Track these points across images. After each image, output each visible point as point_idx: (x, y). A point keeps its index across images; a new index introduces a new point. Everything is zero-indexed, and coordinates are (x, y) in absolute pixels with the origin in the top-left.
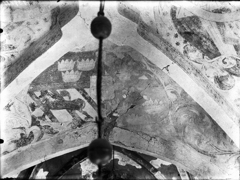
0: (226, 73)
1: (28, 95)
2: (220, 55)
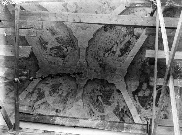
0: (134, 37)
1: (147, 110)
2: (129, 40)
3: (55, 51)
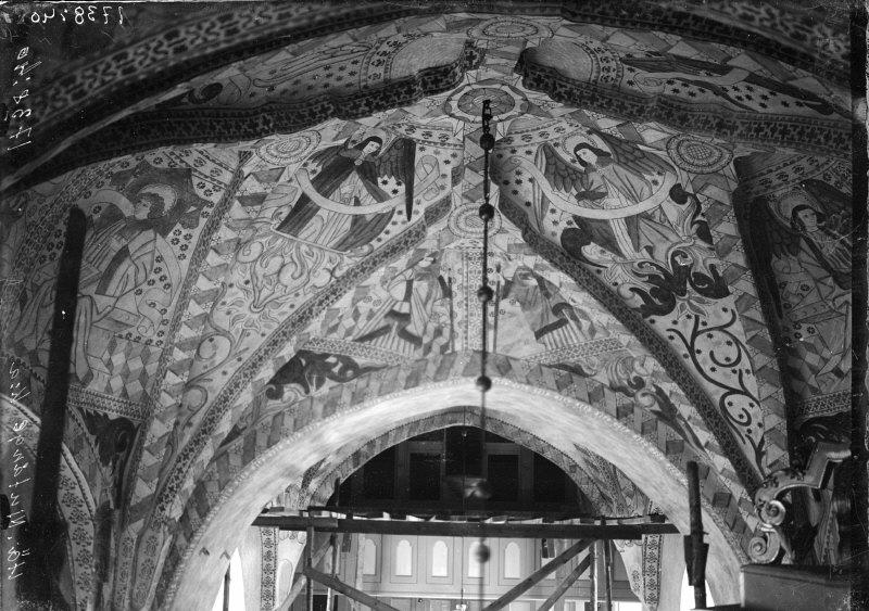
3: (385, 183)
